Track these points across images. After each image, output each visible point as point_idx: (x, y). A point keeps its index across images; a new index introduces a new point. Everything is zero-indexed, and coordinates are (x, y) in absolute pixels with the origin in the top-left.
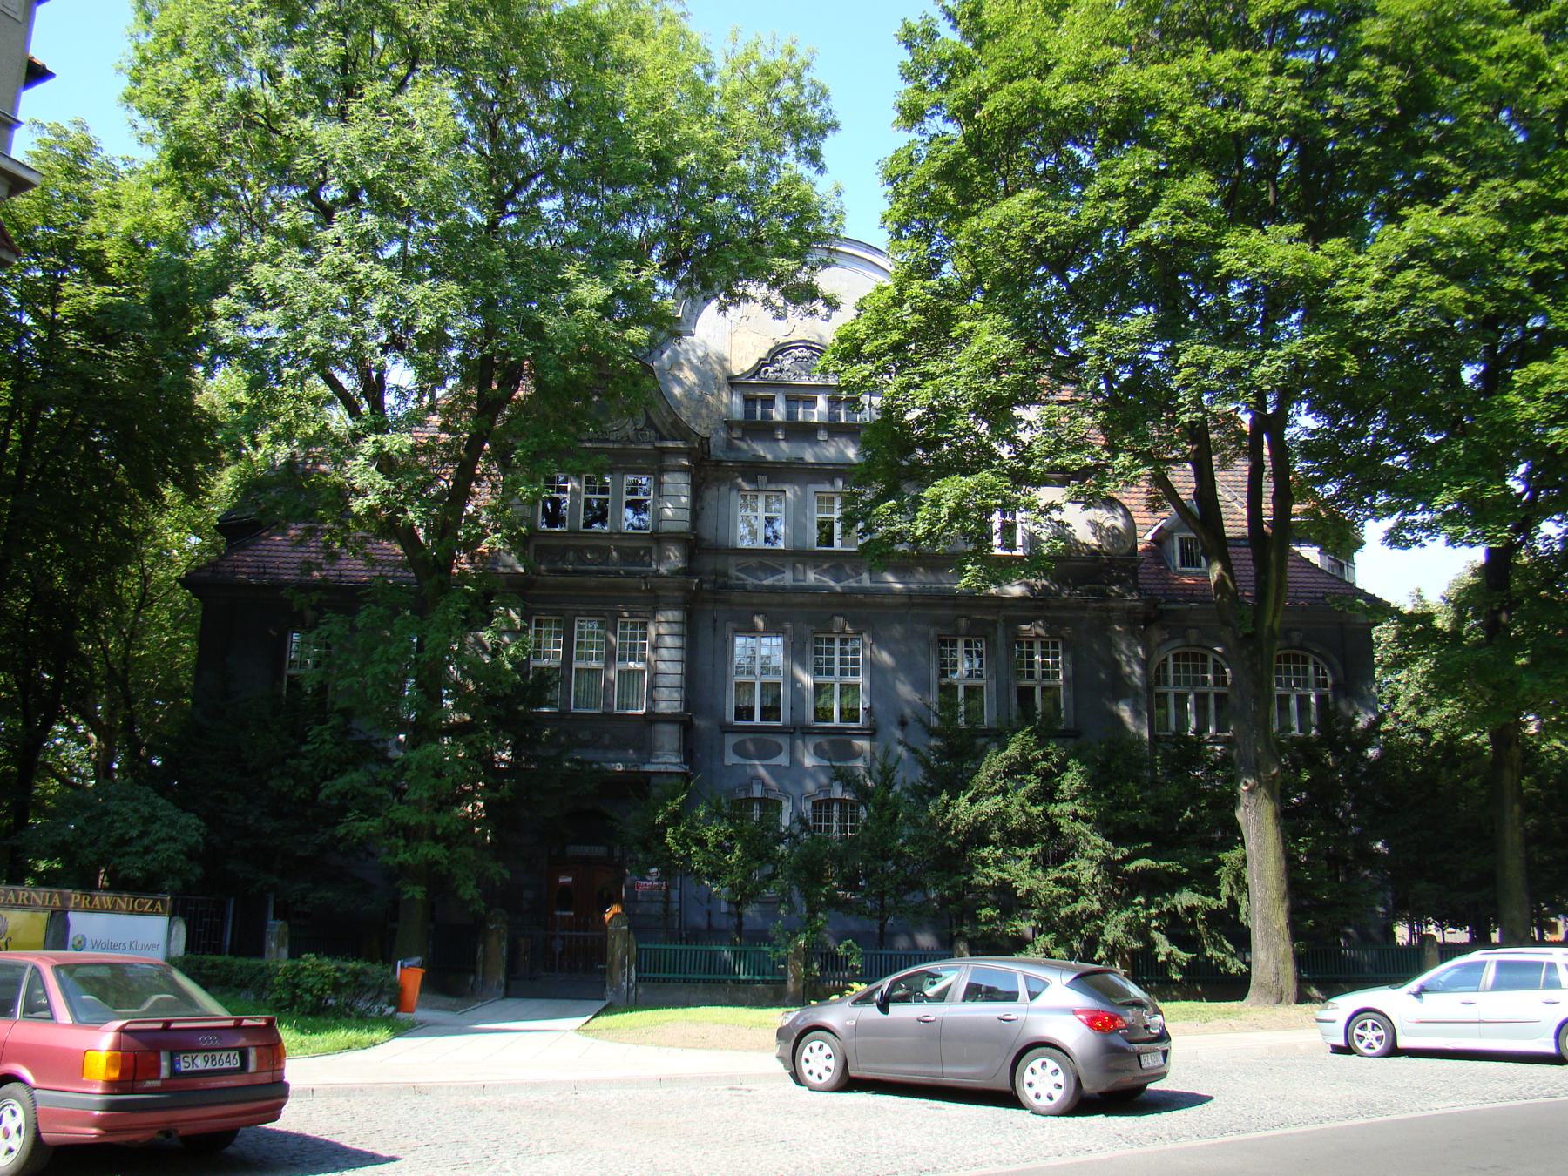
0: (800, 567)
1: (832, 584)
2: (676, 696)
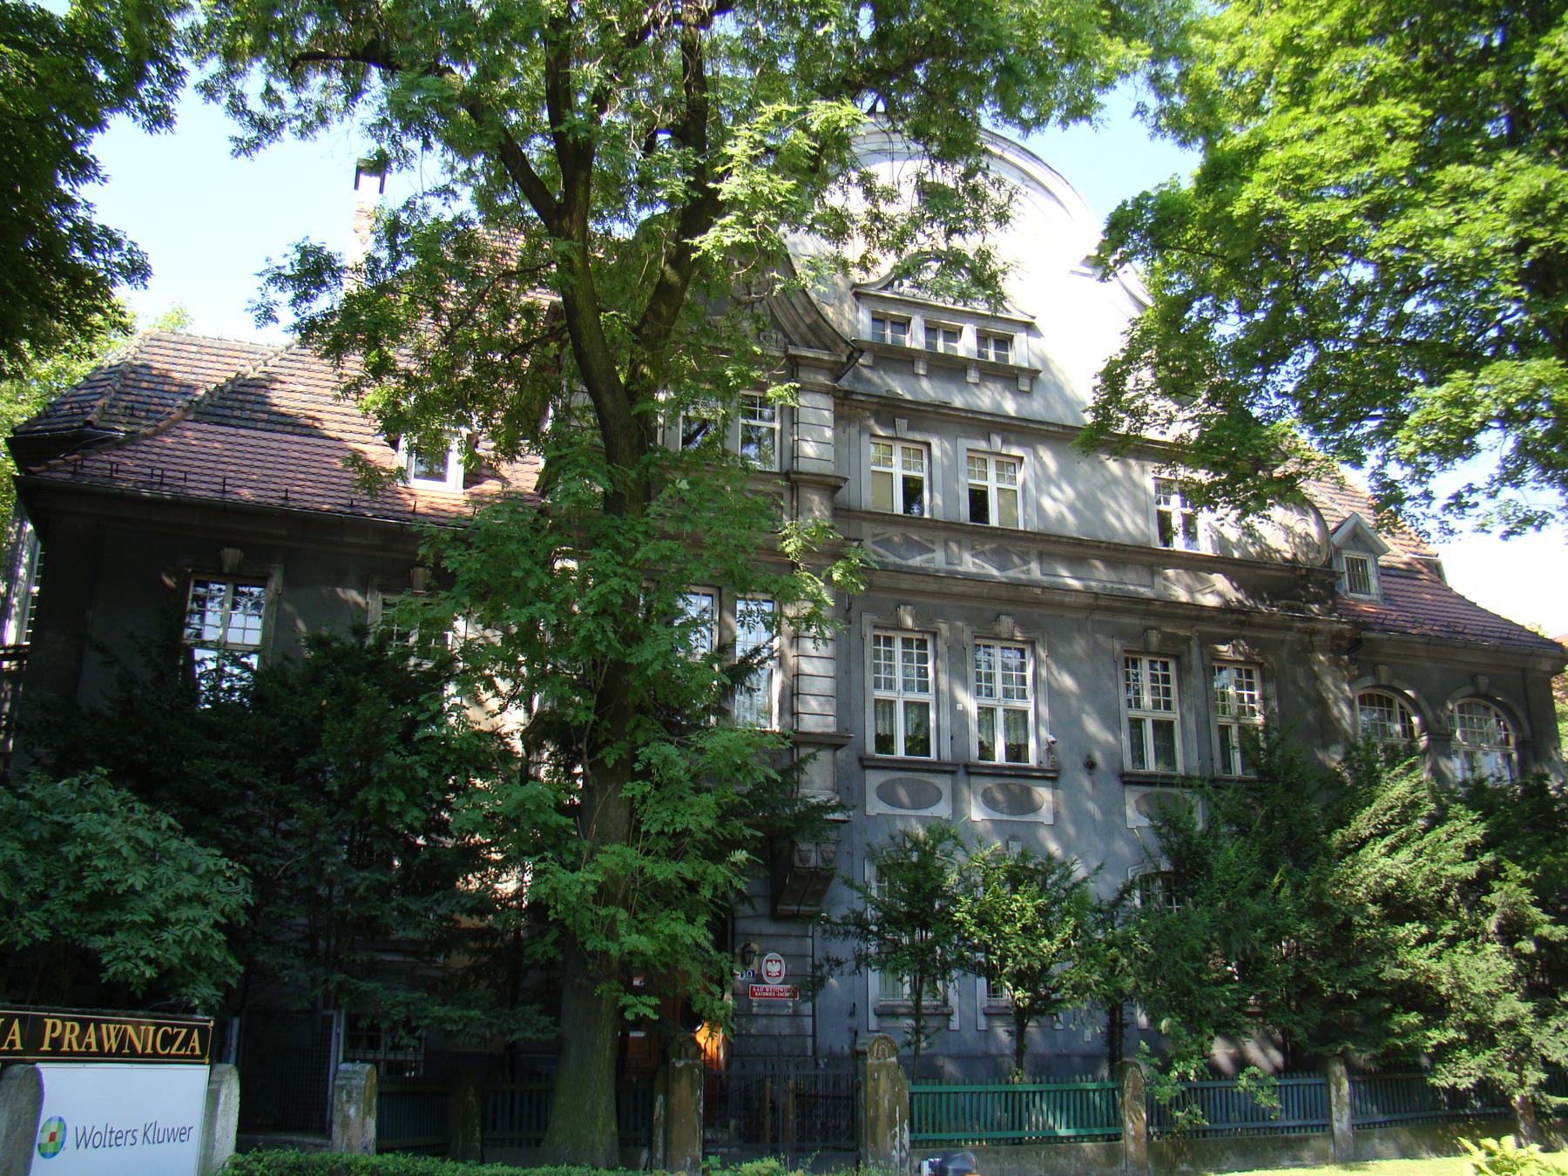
0: (954, 547)
1: (995, 572)
2: (829, 710)
